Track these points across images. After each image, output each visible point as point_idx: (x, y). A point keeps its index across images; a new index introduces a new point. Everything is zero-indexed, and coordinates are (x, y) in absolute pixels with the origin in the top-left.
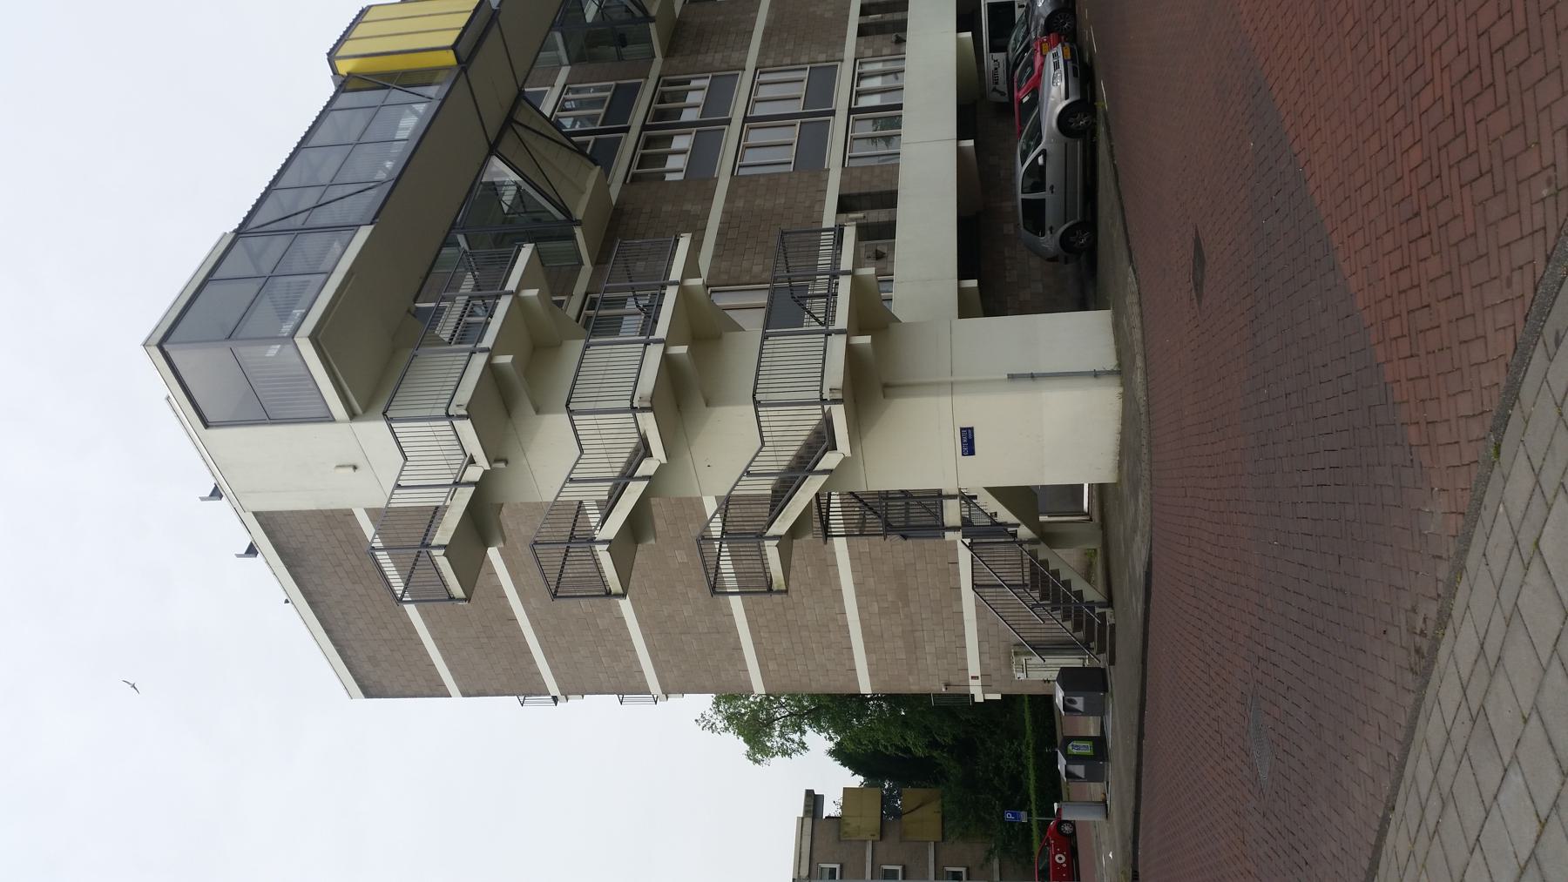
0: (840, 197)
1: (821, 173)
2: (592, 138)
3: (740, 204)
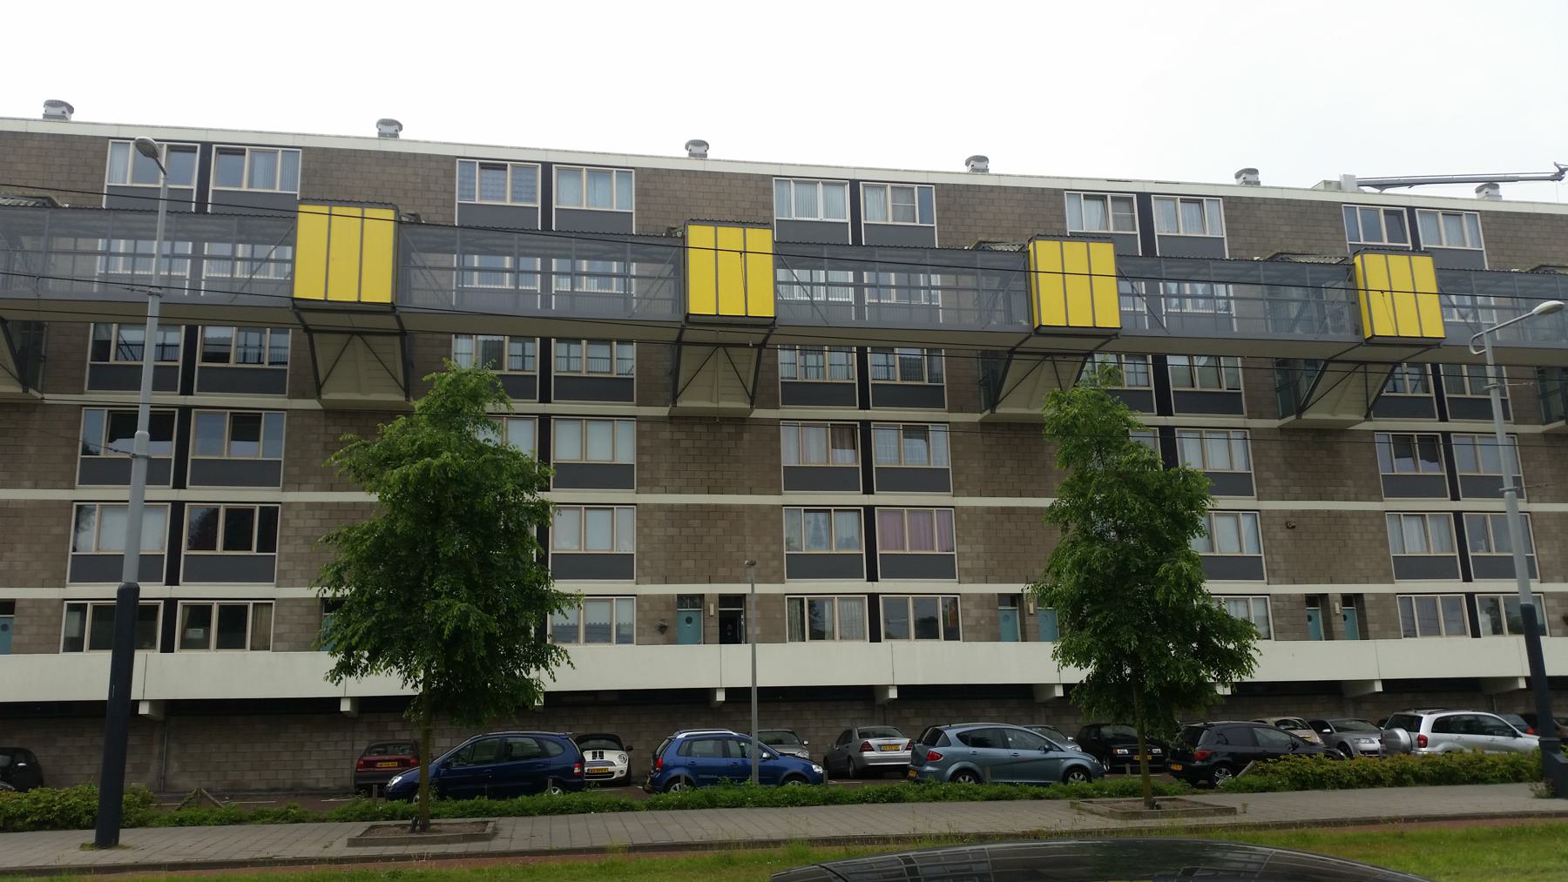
0: (1361, 595)
1: (1386, 578)
2: (1433, 394)
3: (1355, 521)
